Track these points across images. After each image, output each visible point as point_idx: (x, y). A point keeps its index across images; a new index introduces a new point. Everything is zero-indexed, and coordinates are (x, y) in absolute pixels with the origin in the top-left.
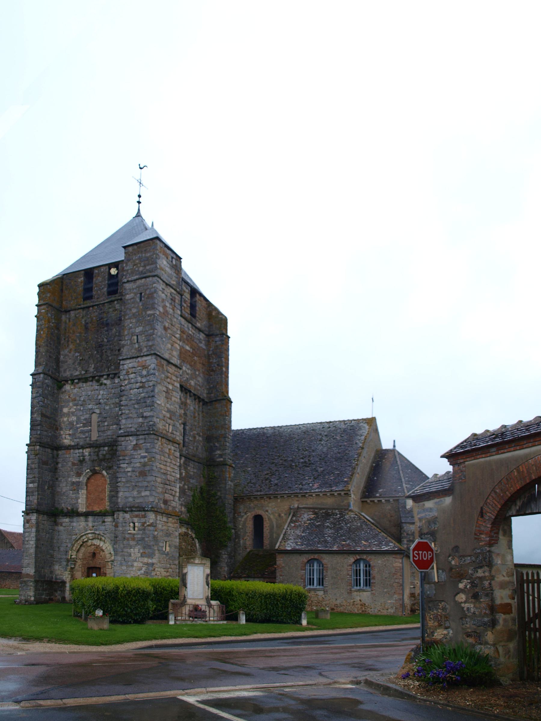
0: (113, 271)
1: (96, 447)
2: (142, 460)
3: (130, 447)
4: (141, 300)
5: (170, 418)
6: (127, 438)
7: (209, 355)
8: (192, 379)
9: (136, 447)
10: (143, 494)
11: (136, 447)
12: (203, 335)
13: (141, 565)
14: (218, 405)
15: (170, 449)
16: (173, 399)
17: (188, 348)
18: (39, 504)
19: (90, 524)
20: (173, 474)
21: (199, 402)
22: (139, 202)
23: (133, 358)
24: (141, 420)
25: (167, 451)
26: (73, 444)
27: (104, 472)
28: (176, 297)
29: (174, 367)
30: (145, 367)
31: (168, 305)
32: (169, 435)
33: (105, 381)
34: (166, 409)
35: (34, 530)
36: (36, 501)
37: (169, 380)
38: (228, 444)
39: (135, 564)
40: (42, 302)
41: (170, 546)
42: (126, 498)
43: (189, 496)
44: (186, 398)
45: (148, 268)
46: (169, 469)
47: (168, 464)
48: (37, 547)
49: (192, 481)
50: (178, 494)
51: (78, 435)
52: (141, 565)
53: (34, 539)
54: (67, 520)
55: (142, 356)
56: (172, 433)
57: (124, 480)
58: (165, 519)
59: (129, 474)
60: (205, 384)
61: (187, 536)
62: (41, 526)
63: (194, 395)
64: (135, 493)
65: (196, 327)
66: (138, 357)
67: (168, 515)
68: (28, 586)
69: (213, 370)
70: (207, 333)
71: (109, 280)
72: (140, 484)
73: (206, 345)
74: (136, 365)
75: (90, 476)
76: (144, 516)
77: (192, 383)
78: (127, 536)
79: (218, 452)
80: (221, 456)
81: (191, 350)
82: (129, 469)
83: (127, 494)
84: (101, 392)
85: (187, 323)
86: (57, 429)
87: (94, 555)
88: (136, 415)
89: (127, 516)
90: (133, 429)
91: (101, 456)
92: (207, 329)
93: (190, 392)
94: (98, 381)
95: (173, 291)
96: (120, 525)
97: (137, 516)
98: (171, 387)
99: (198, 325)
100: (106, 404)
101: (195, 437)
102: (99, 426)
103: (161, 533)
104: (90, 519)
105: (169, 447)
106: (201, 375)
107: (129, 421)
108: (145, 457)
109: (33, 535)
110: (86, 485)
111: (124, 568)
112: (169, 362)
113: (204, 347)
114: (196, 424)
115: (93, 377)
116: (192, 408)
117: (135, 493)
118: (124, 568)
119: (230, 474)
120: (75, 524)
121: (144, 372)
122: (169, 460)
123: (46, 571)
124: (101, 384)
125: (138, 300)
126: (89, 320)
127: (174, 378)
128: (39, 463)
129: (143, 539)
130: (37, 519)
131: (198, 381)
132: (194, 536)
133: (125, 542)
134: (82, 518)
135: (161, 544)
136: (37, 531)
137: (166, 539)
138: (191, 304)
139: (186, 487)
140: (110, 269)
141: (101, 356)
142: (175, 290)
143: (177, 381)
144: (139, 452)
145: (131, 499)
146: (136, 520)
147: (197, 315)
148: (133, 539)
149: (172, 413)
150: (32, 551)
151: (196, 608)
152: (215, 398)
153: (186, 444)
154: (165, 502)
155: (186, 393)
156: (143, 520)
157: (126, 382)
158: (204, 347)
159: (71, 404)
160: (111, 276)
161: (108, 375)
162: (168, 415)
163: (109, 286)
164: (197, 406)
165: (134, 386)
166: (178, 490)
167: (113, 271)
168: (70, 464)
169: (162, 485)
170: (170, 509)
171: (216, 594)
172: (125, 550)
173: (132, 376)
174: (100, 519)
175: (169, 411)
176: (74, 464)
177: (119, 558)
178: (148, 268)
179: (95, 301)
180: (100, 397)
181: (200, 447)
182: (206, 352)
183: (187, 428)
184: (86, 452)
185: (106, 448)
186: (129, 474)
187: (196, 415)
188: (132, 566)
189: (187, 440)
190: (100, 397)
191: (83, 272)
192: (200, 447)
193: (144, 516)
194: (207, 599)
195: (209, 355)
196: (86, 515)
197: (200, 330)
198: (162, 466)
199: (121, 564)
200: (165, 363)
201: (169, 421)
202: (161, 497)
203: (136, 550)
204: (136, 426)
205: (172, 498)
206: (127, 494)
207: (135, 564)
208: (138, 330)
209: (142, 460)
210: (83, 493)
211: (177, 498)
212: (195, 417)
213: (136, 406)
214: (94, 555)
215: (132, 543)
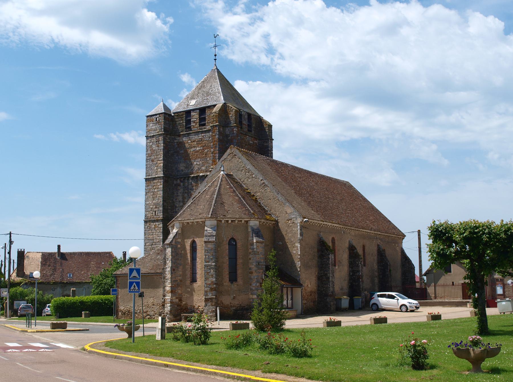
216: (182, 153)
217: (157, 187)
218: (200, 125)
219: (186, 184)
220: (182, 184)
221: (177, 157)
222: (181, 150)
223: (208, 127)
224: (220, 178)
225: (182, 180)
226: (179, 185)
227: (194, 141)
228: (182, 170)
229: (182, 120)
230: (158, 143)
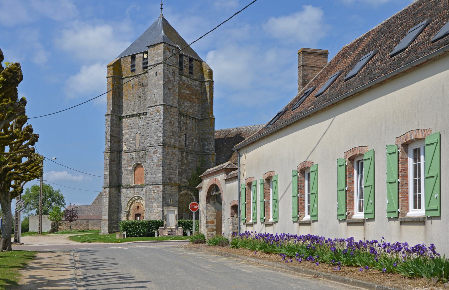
0: (145, 56)
1: (138, 151)
2: (157, 159)
3: (152, 152)
4: (156, 76)
5: (173, 136)
6: (151, 148)
7: (202, 93)
8: (190, 108)
9: (155, 152)
10: (158, 176)
11: (155, 152)
12: (198, 82)
13: (157, 211)
14: (206, 121)
15: (172, 152)
16: (174, 125)
17: (188, 92)
18: (110, 183)
19: (136, 192)
20: (175, 164)
21: (196, 120)
22: (161, 8)
23: (153, 106)
24: (157, 138)
25: (171, 153)
26: (127, 150)
27: (142, 164)
28: (176, 70)
29: (174, 109)
30: (159, 111)
31: (170, 76)
32: (172, 144)
33: (142, 116)
34: (170, 131)
35: (108, 196)
36: (109, 181)
37: (171, 116)
38: (211, 142)
39: (155, 211)
40: (110, 75)
41: (173, 201)
42: (151, 178)
43: (189, 173)
44: (187, 120)
45: (159, 58)
46: (172, 162)
47: (171, 159)
48: (109, 205)
49: (190, 165)
50: (177, 174)
51: (129, 145)
52: (157, 211)
53: (108, 201)
54: (125, 190)
55: (157, 106)
56: (174, 143)
57: (149, 169)
58: (169, 188)
59: (152, 166)
60: (200, 109)
61: (188, 195)
62: (112, 194)
63: (192, 117)
64: (155, 175)
65: (193, 79)
66: (155, 106)
67: (172, 185)
68: (398, 259)
69: (204, 102)
70: (200, 80)
71: (143, 60)
72: (156, 171)
73: (200, 87)
74: (154, 110)
75: (136, 166)
76: (159, 187)
77: (191, 111)
78: (151, 197)
79: (207, 147)
80: (208, 149)
81: (190, 93)
82: (152, 164)
83: (151, 176)
84: (141, 122)
85: (187, 78)
86: (119, 142)
87: (138, 207)
88: (154, 136)
89: (151, 187)
90: (153, 143)
91: (141, 156)
92: (201, 78)
93: (189, 116)
94: (139, 116)
95: (174, 68)
96: (148, 192)
97: (155, 187)
98: (173, 119)
99: (195, 77)
100: (143, 128)
101: (193, 140)
102: (140, 140)
103: (167, 195)
104: (136, 189)
105: (172, 150)
106: (197, 105)
107: (152, 139)
108: (158, 157)
109: (108, 199)
110: (135, 171)
111: (150, 213)
112: (171, 107)
113: (199, 89)
114: (193, 133)
115: (136, 114)
116: (190, 125)
117: (155, 175)
118: (150, 213)
119: (213, 159)
120: (128, 192)
121: (158, 114)
122: (172, 157)
123: (115, 217)
124: (141, 118)
125: (155, 75)
126: (134, 83)
127: (175, 114)
128: (110, 161)
129: (158, 198)
130: (109, 191)
131: (195, 109)
132: (192, 194)
133: (150, 200)
134: (133, 189)
135: (167, 201)
136: (110, 197)
137: (170, 198)
138: (189, 67)
139: (187, 168)
140: (143, 55)
141: (140, 103)
142: (175, 67)
143: (177, 115)
144: (156, 154)
145: (152, 179)
146: (155, 189)
147: (194, 72)
148: (154, 199)
149: (174, 133)
150: (107, 207)
151: (172, 230)
152: (206, 116)
153: (187, 145)
154: (170, 179)
155: (187, 117)
156: (158, 189)
157: (150, 119)
158: (199, 89)
159: (126, 128)
160: (144, 59)
161: (144, 113)
162: (171, 134)
163: (144, 64)
164: (194, 123)
165: (154, 121)
166: (178, 172)
167: (145, 56)
168: (126, 160)
169: (168, 171)
170: (173, 182)
171: (180, 224)
172: (150, 204)
173: (153, 115)
174: (141, 189)
175: (172, 132)
176: (128, 161)
177: (147, 209)
178: (159, 58)
179: (137, 73)
180: (140, 125)
181: (196, 145)
182: (200, 92)
183: (188, 136)
184: (134, 154)
185: (143, 152)
186: (152, 166)
187: (194, 128)
188: (153, 212)
189: (187, 143)
190: (140, 125)
191: (130, 57)
192: (196, 145)
193: (159, 187)
194: (176, 226)
195: (202, 93)
196: (134, 187)
197: (196, 80)
198: (167, 161)
199: (148, 212)
200: (169, 107)
201: (172, 137)
202: (168, 177)
203: (155, 204)
204: (154, 141)
205: (174, 177)
206: (151, 176)
207: (155, 211)
208: (155, 91)
209: (157, 159)
210: (132, 175)
211: (177, 176)
212: (192, 130)
213: (155, 131)
214: (138, 207)
215: (153, 200)
217: (174, 116)
227: (185, 84)
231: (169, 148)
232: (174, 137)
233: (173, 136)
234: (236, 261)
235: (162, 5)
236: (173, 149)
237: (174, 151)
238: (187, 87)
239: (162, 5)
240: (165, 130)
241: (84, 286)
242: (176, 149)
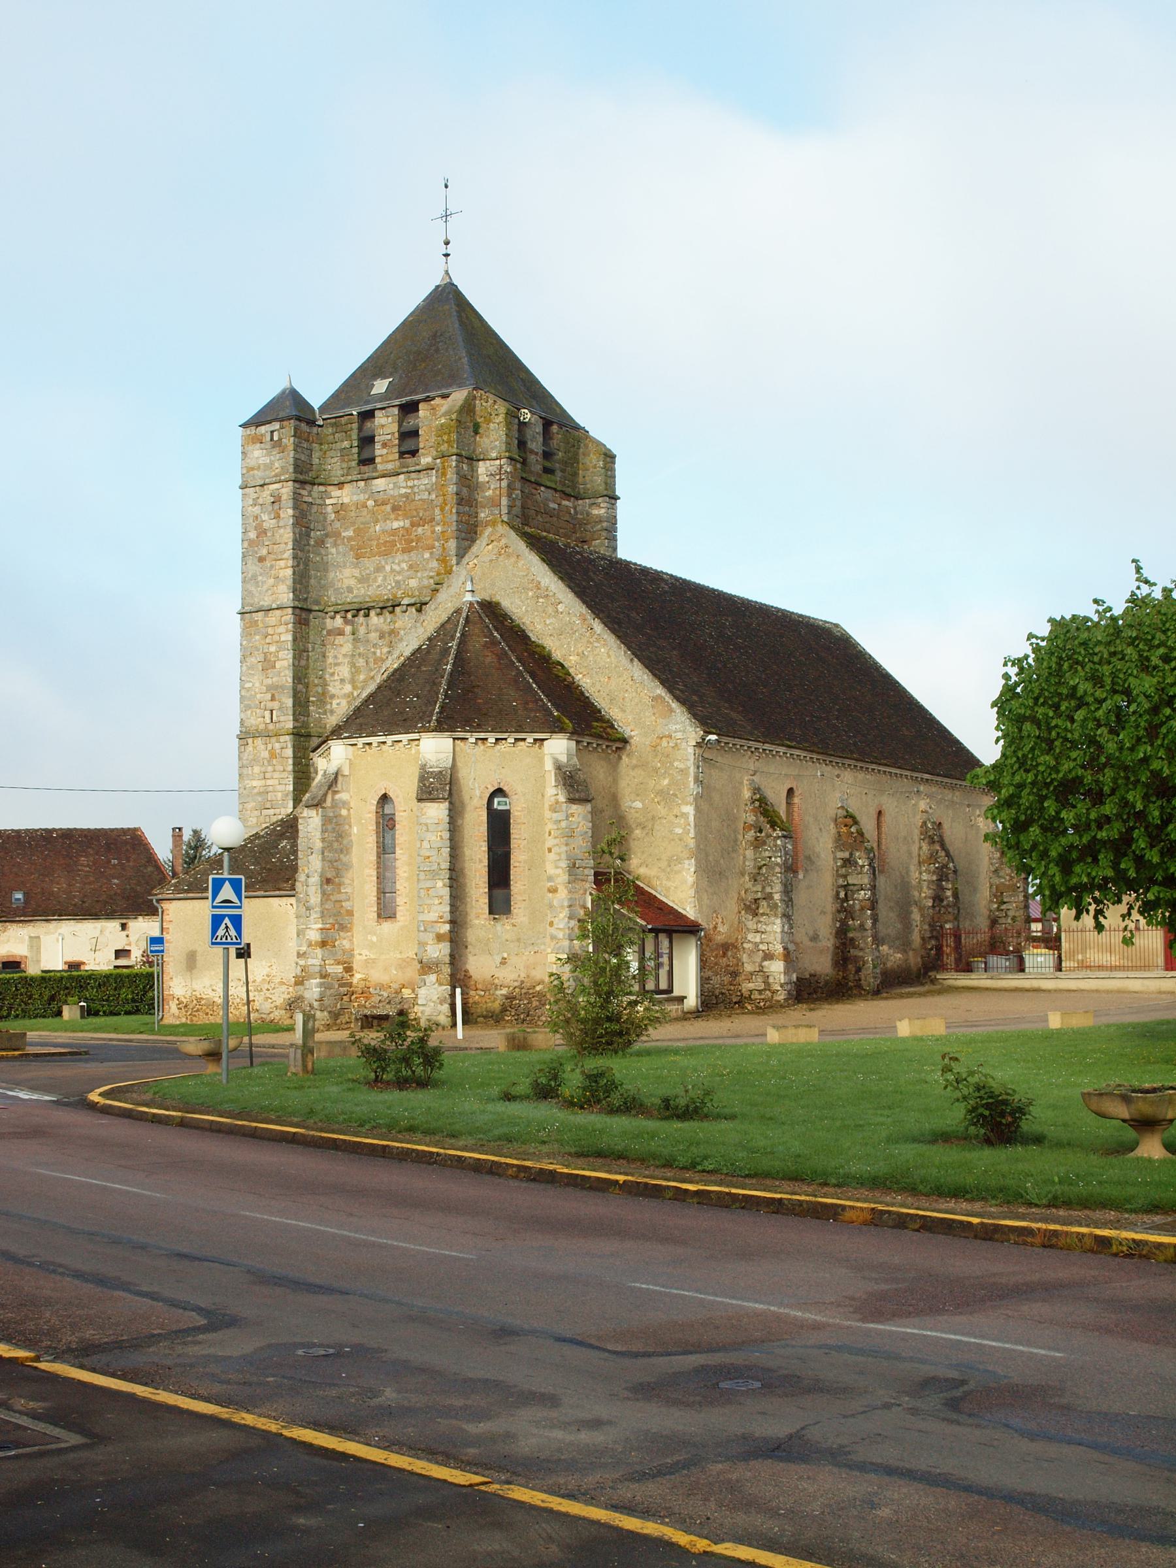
29: (278, 612)
32: (271, 727)
98: (273, 649)
122: (270, 768)
169: (257, 813)
198: (255, 783)
216: (350, 539)
217: (276, 638)
218: (402, 454)
219: (362, 630)
220: (348, 629)
221: (333, 550)
222: (346, 529)
223: (425, 460)
224: (464, 615)
225: (349, 615)
226: (341, 633)
227: (384, 503)
228: (350, 590)
229: (349, 438)
230: (276, 506)
231: (259, 741)
232: (275, 705)
233: (273, 699)
234: (978, 1426)
235: (447, 243)
236: (274, 739)
237: (277, 746)
238: (395, 509)
239: (447, 243)
240: (248, 690)
241: (314, 1345)
242: (282, 739)
